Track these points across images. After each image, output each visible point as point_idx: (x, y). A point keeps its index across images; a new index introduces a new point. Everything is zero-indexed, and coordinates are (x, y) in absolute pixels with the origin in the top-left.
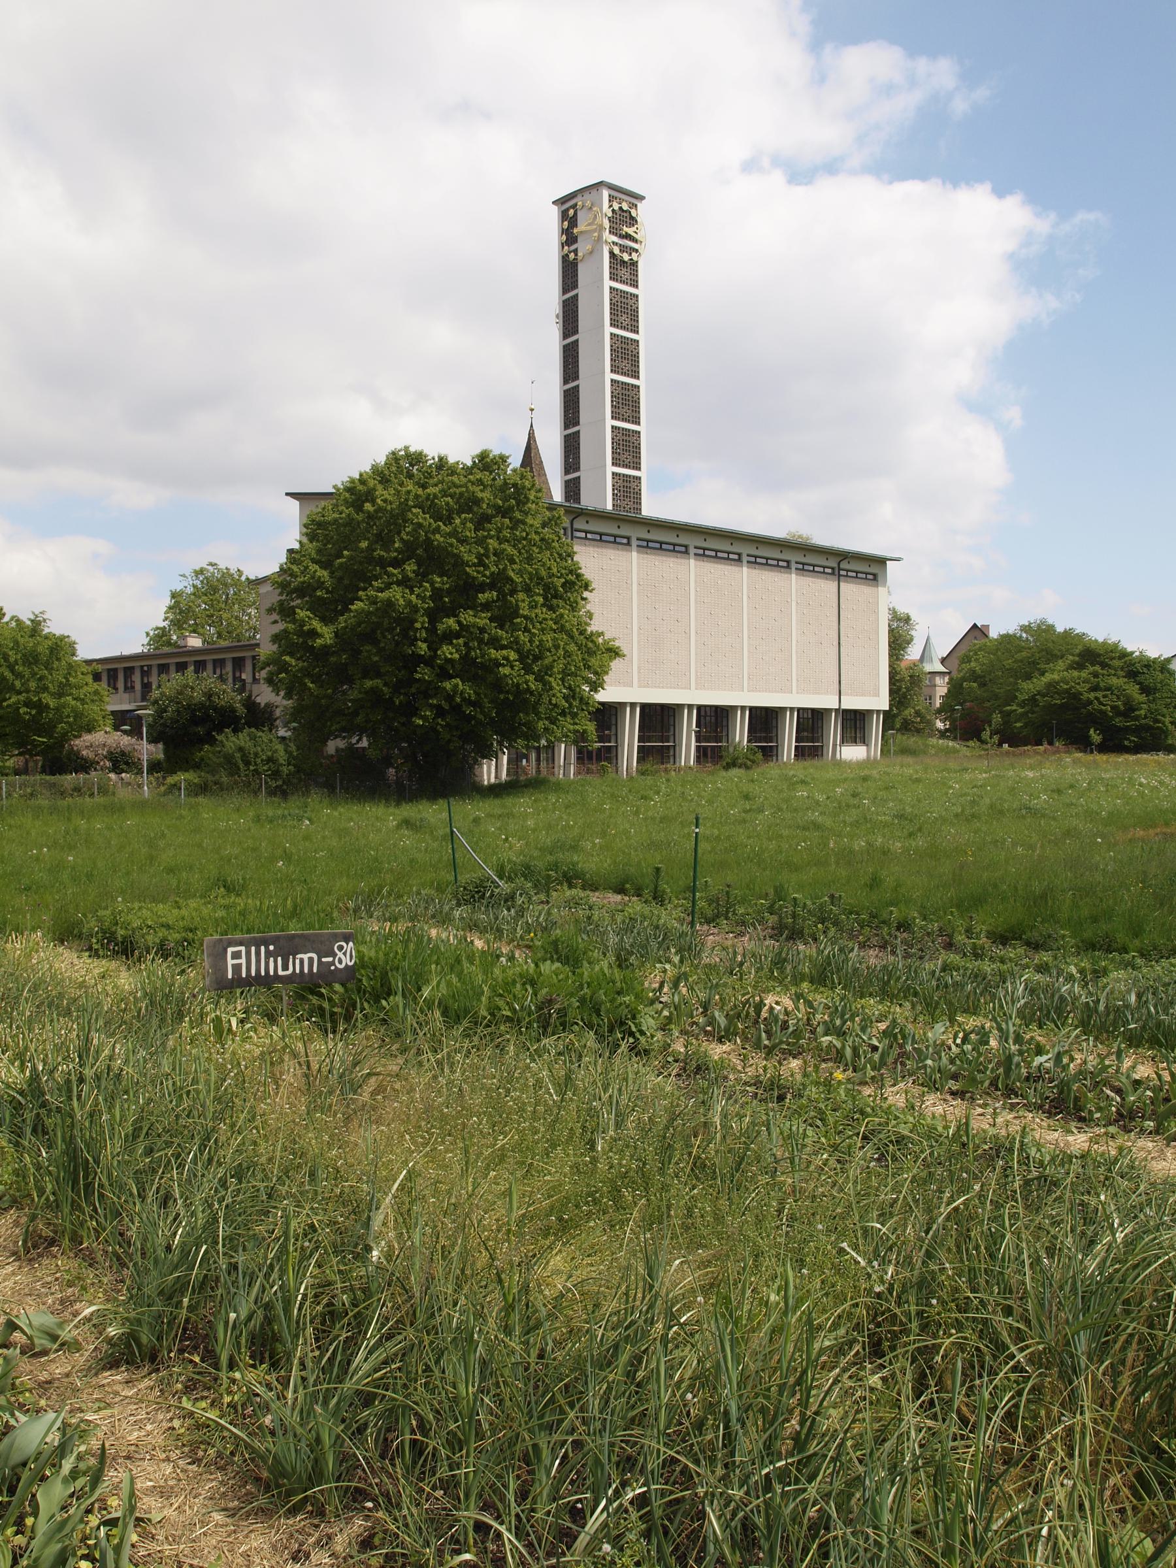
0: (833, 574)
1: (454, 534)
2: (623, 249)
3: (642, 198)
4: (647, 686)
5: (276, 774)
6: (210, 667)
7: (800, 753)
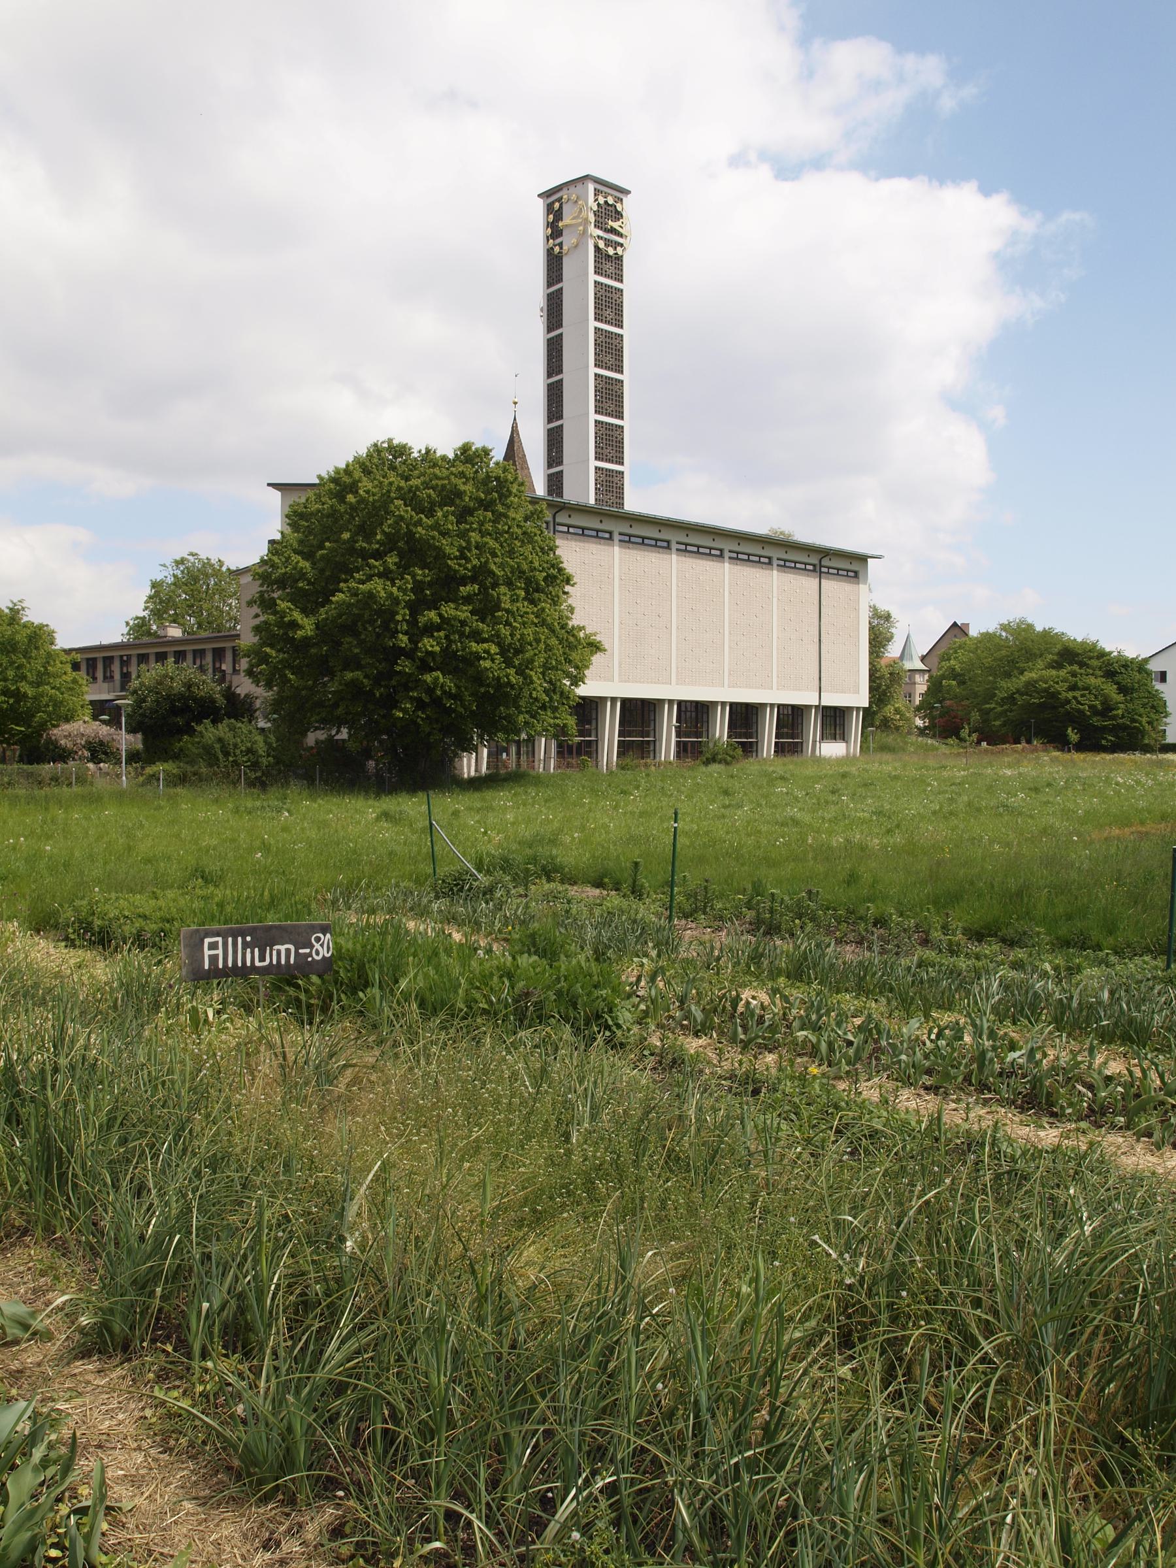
0: (814, 570)
1: (436, 526)
2: (608, 243)
3: (627, 192)
5: (255, 765)
6: (190, 657)
7: (780, 749)
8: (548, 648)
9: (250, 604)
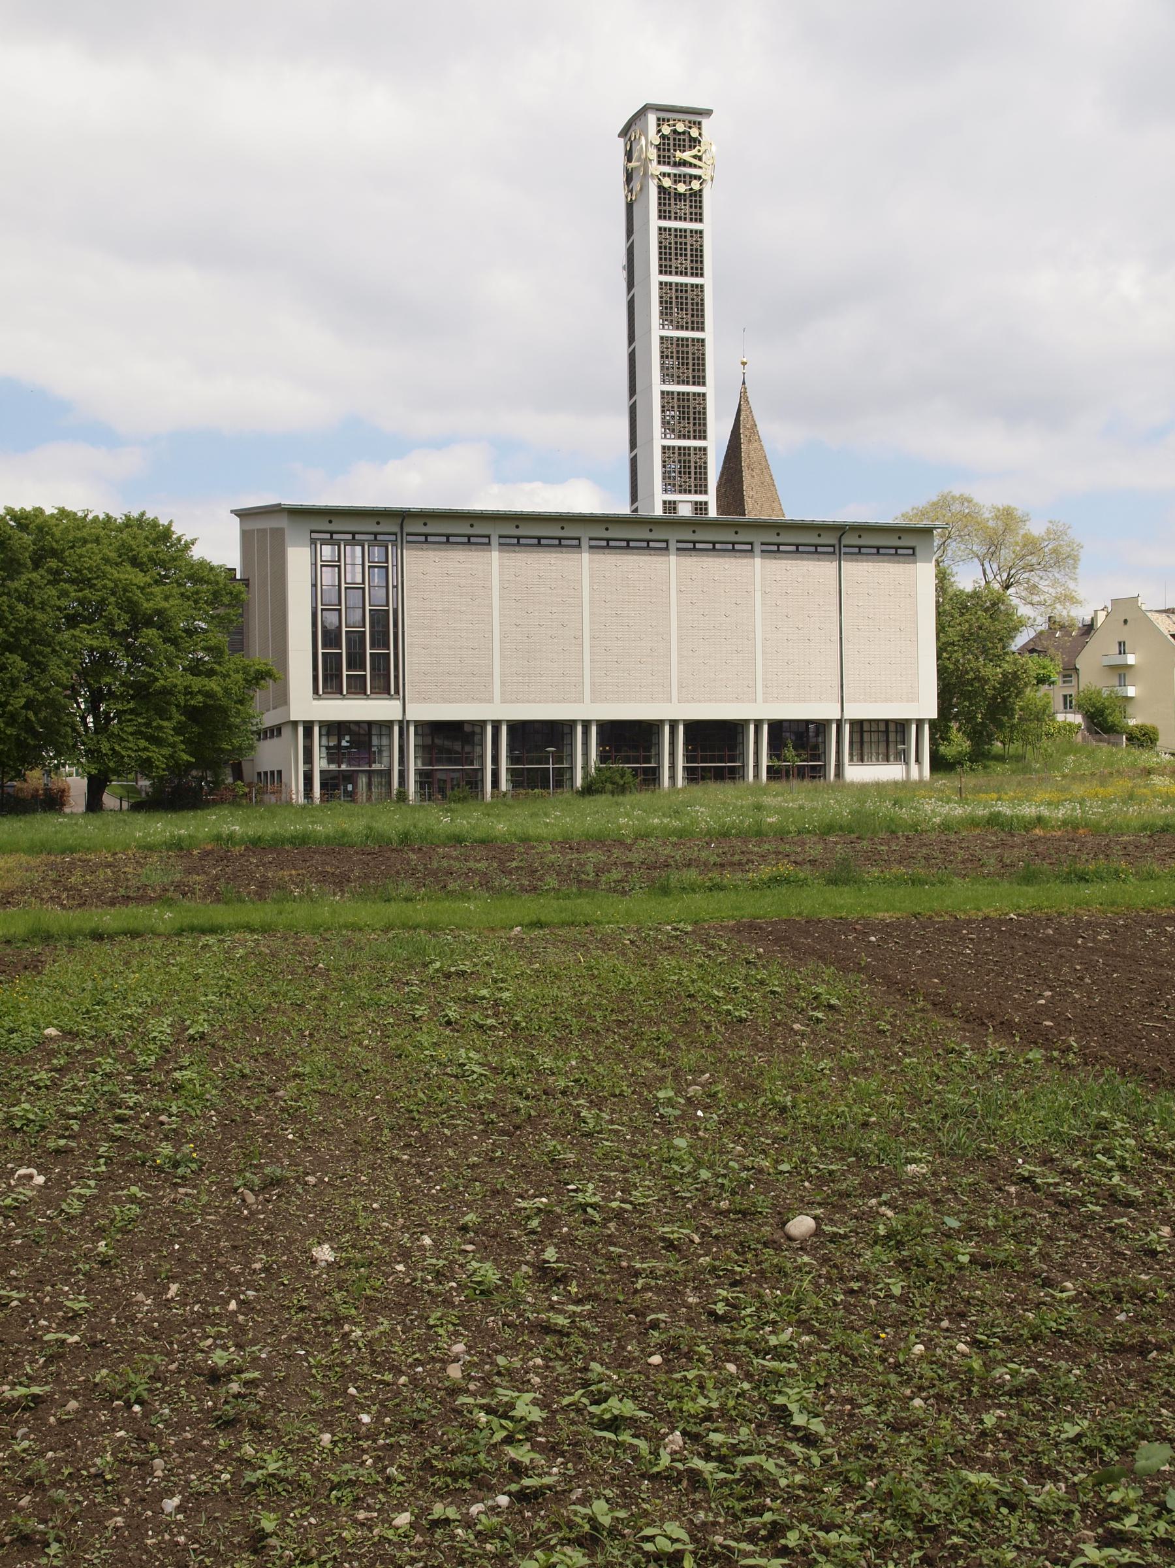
0: (834, 553)
2: (677, 178)
3: (708, 113)
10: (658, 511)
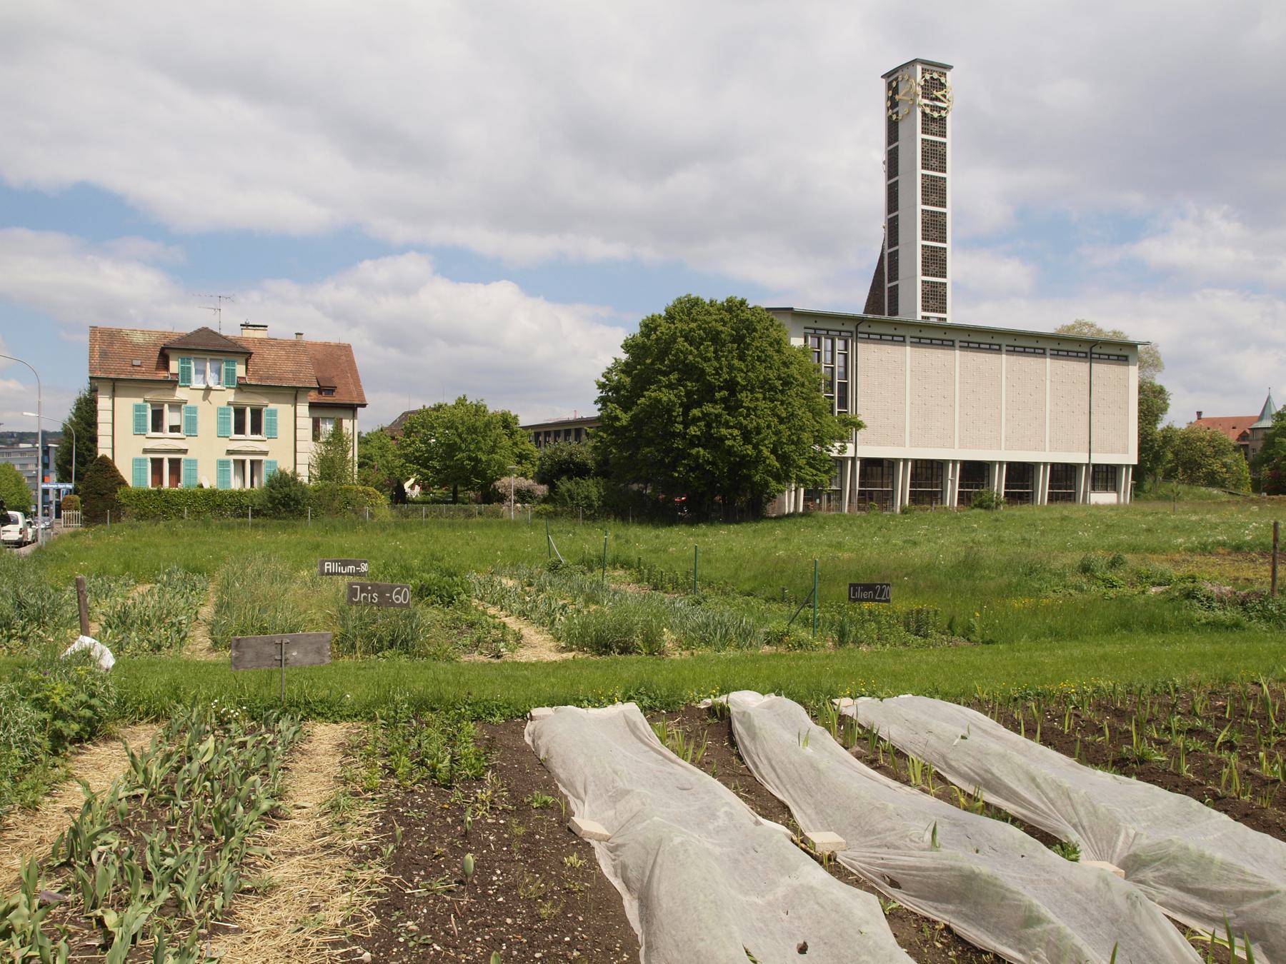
1: (700, 355)
2: (934, 108)
4: (918, 446)
5: (590, 506)
6: (562, 435)
7: (1053, 497)
8: (777, 433)
9: (596, 402)
10: (919, 318)
